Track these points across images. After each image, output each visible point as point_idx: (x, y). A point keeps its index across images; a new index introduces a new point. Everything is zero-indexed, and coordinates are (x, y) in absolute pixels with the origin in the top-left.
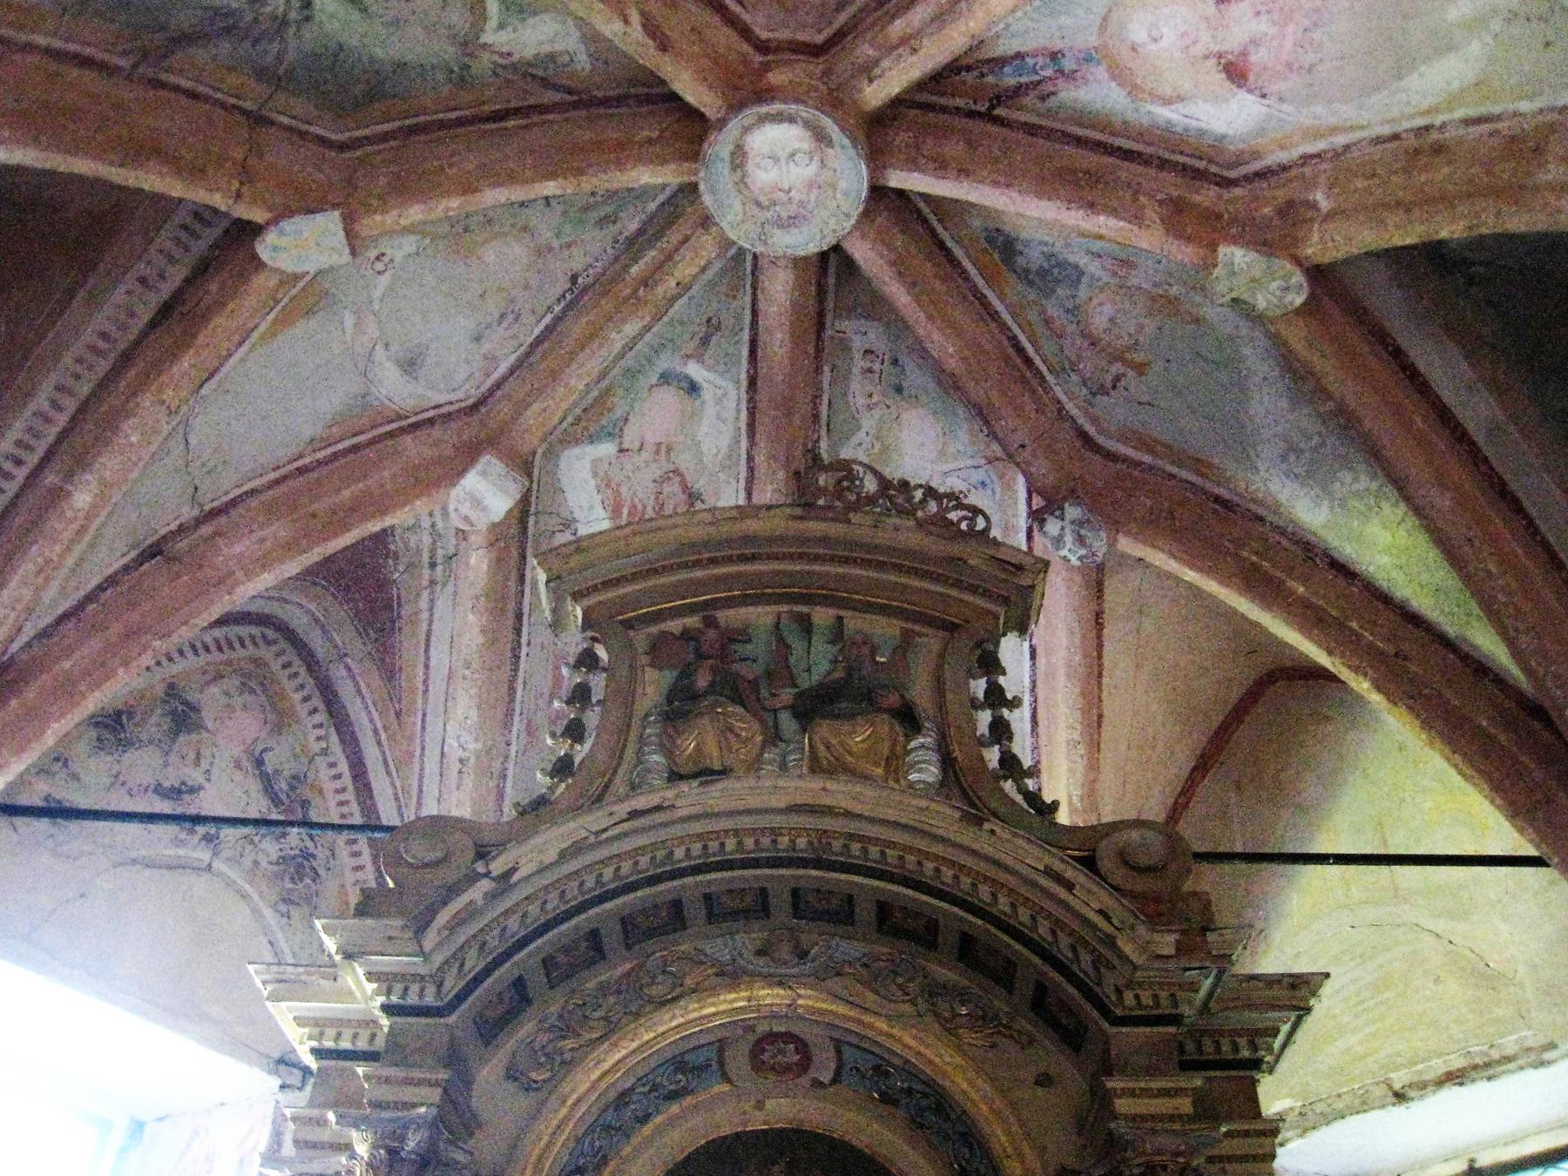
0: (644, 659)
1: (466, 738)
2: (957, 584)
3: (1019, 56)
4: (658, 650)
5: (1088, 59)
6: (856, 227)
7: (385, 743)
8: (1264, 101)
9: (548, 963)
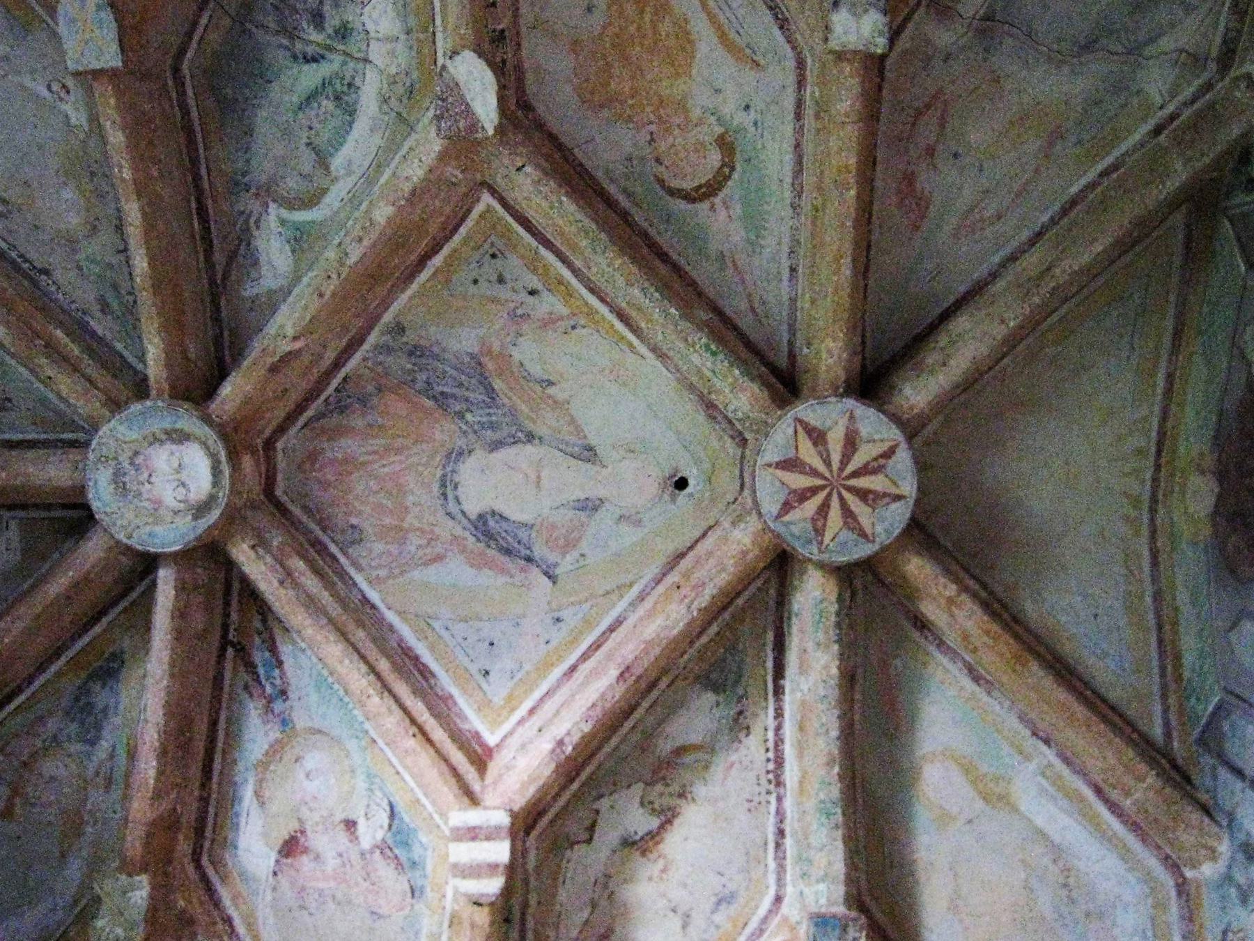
3: (280, 664)
5: (284, 722)
6: (118, 542)
8: (271, 876)
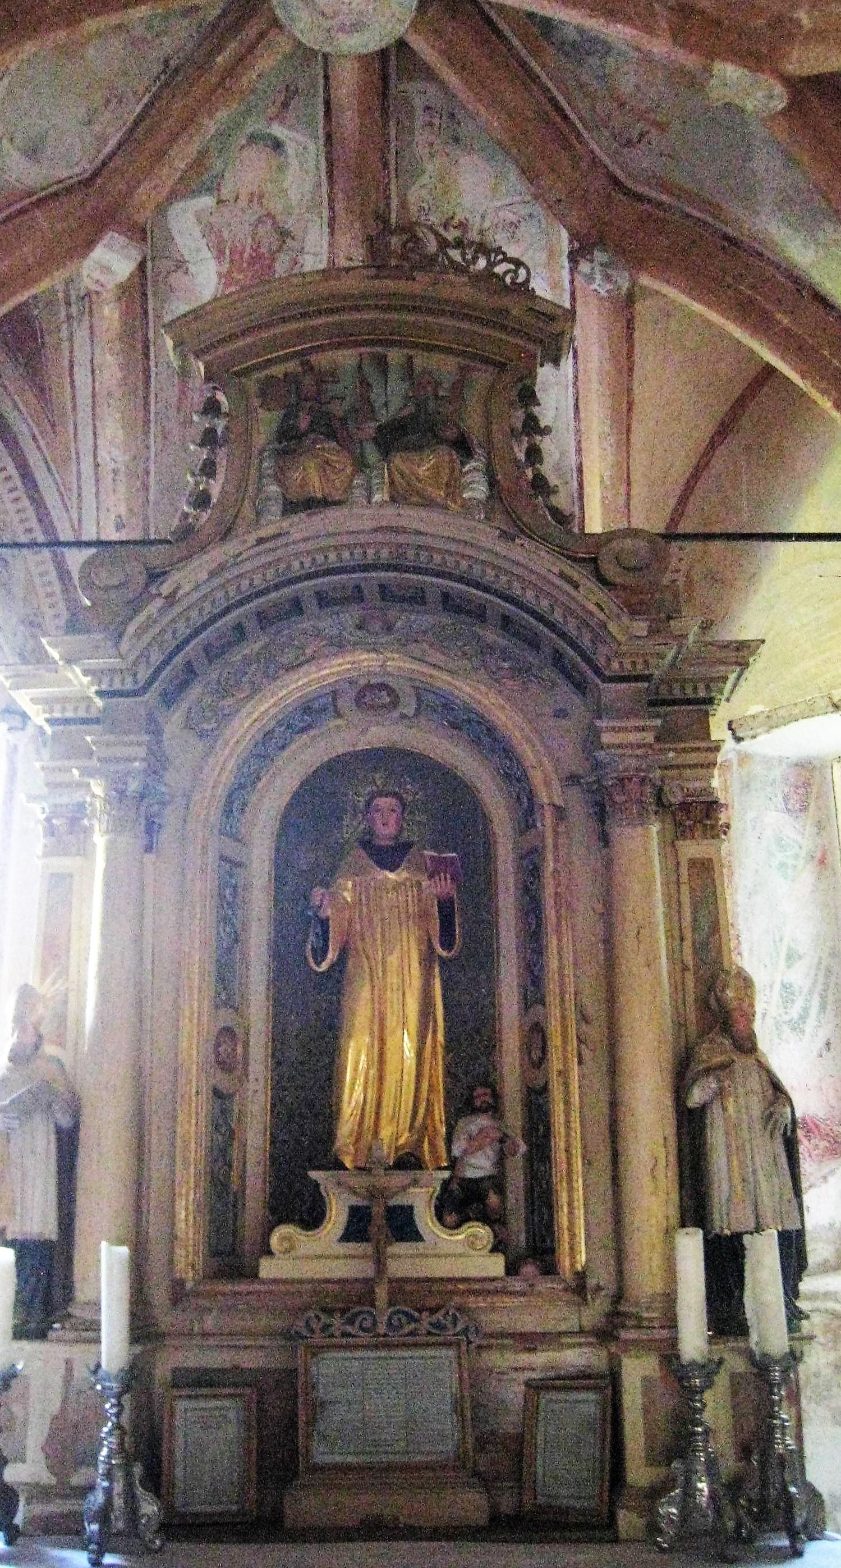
0: (256, 402)
1: (116, 453)
2: (504, 328)
4: (267, 390)
7: (44, 448)
9: (207, 649)
